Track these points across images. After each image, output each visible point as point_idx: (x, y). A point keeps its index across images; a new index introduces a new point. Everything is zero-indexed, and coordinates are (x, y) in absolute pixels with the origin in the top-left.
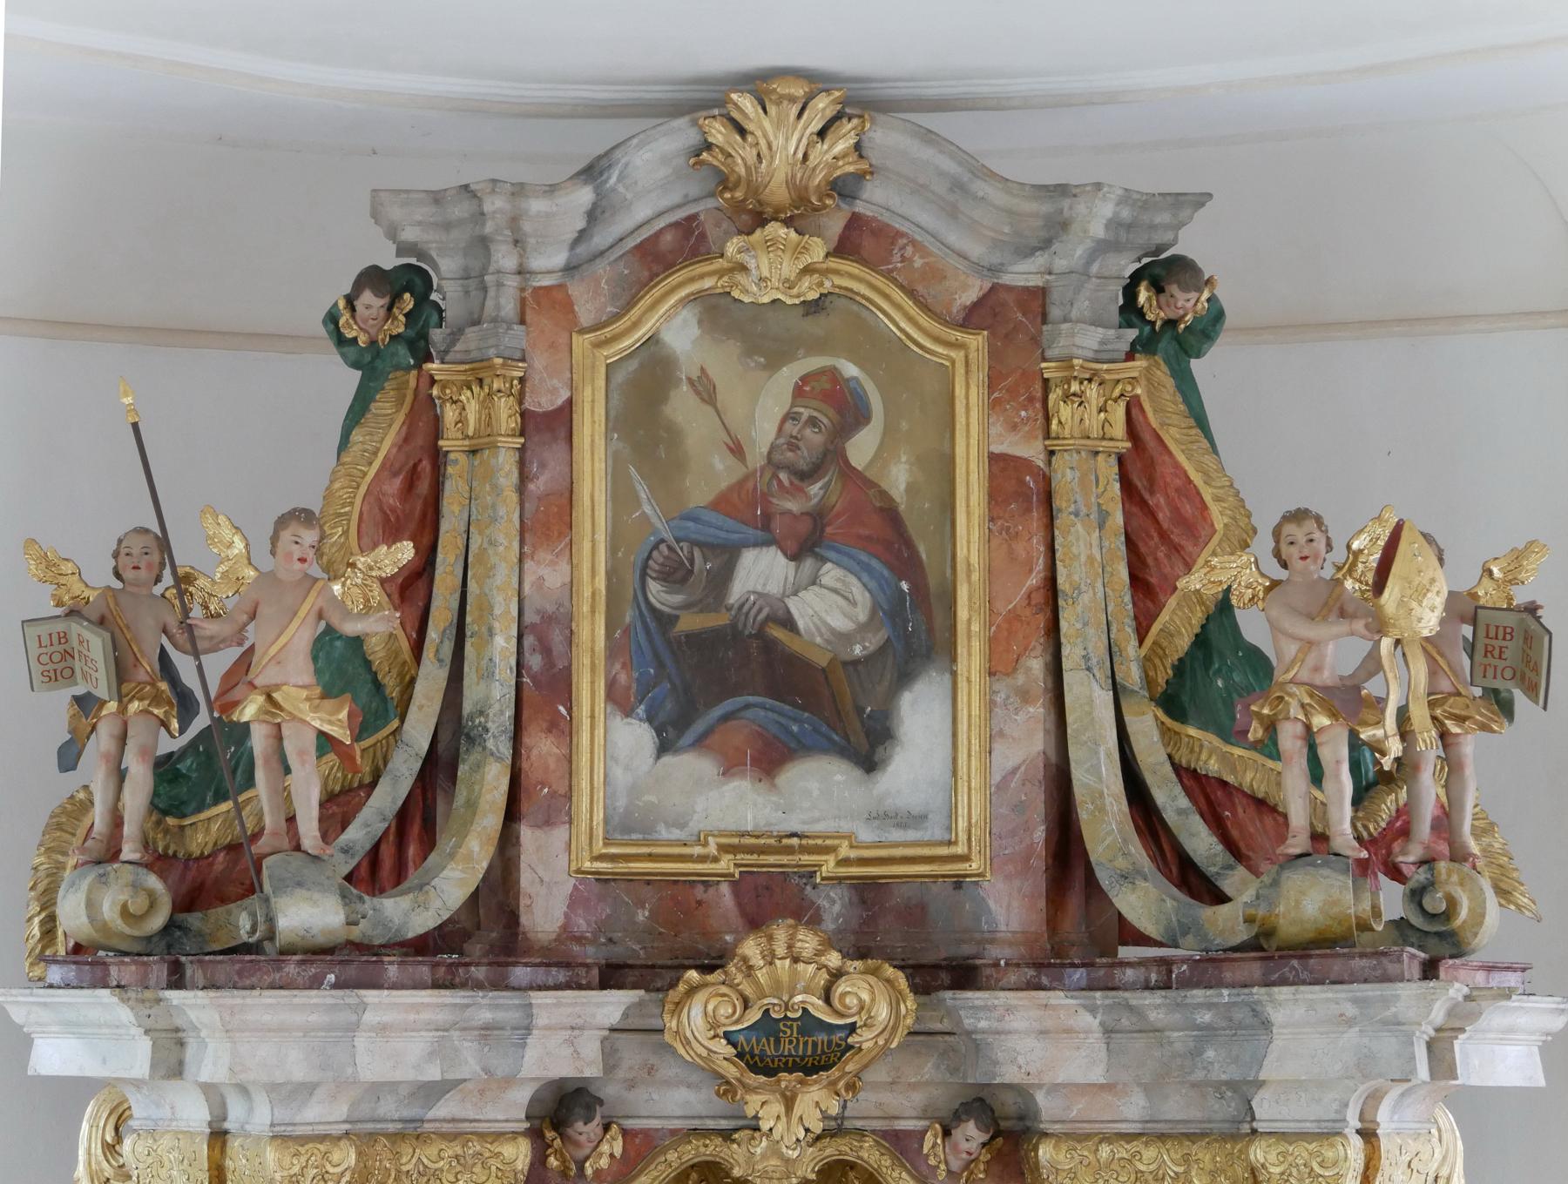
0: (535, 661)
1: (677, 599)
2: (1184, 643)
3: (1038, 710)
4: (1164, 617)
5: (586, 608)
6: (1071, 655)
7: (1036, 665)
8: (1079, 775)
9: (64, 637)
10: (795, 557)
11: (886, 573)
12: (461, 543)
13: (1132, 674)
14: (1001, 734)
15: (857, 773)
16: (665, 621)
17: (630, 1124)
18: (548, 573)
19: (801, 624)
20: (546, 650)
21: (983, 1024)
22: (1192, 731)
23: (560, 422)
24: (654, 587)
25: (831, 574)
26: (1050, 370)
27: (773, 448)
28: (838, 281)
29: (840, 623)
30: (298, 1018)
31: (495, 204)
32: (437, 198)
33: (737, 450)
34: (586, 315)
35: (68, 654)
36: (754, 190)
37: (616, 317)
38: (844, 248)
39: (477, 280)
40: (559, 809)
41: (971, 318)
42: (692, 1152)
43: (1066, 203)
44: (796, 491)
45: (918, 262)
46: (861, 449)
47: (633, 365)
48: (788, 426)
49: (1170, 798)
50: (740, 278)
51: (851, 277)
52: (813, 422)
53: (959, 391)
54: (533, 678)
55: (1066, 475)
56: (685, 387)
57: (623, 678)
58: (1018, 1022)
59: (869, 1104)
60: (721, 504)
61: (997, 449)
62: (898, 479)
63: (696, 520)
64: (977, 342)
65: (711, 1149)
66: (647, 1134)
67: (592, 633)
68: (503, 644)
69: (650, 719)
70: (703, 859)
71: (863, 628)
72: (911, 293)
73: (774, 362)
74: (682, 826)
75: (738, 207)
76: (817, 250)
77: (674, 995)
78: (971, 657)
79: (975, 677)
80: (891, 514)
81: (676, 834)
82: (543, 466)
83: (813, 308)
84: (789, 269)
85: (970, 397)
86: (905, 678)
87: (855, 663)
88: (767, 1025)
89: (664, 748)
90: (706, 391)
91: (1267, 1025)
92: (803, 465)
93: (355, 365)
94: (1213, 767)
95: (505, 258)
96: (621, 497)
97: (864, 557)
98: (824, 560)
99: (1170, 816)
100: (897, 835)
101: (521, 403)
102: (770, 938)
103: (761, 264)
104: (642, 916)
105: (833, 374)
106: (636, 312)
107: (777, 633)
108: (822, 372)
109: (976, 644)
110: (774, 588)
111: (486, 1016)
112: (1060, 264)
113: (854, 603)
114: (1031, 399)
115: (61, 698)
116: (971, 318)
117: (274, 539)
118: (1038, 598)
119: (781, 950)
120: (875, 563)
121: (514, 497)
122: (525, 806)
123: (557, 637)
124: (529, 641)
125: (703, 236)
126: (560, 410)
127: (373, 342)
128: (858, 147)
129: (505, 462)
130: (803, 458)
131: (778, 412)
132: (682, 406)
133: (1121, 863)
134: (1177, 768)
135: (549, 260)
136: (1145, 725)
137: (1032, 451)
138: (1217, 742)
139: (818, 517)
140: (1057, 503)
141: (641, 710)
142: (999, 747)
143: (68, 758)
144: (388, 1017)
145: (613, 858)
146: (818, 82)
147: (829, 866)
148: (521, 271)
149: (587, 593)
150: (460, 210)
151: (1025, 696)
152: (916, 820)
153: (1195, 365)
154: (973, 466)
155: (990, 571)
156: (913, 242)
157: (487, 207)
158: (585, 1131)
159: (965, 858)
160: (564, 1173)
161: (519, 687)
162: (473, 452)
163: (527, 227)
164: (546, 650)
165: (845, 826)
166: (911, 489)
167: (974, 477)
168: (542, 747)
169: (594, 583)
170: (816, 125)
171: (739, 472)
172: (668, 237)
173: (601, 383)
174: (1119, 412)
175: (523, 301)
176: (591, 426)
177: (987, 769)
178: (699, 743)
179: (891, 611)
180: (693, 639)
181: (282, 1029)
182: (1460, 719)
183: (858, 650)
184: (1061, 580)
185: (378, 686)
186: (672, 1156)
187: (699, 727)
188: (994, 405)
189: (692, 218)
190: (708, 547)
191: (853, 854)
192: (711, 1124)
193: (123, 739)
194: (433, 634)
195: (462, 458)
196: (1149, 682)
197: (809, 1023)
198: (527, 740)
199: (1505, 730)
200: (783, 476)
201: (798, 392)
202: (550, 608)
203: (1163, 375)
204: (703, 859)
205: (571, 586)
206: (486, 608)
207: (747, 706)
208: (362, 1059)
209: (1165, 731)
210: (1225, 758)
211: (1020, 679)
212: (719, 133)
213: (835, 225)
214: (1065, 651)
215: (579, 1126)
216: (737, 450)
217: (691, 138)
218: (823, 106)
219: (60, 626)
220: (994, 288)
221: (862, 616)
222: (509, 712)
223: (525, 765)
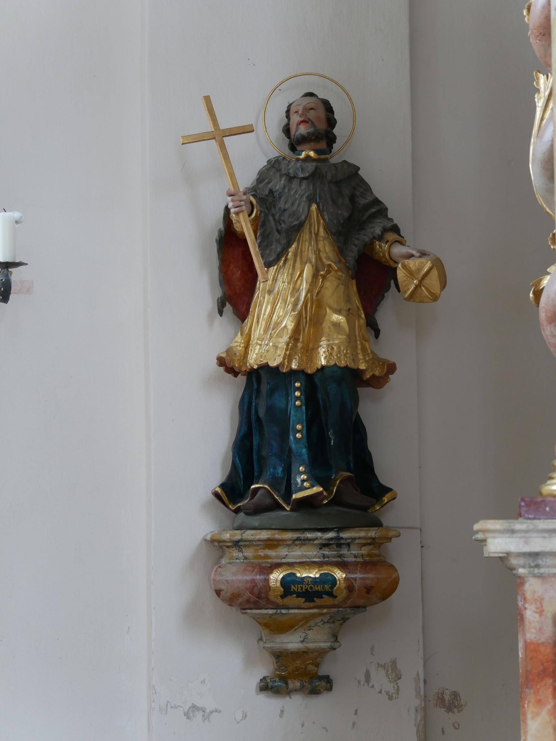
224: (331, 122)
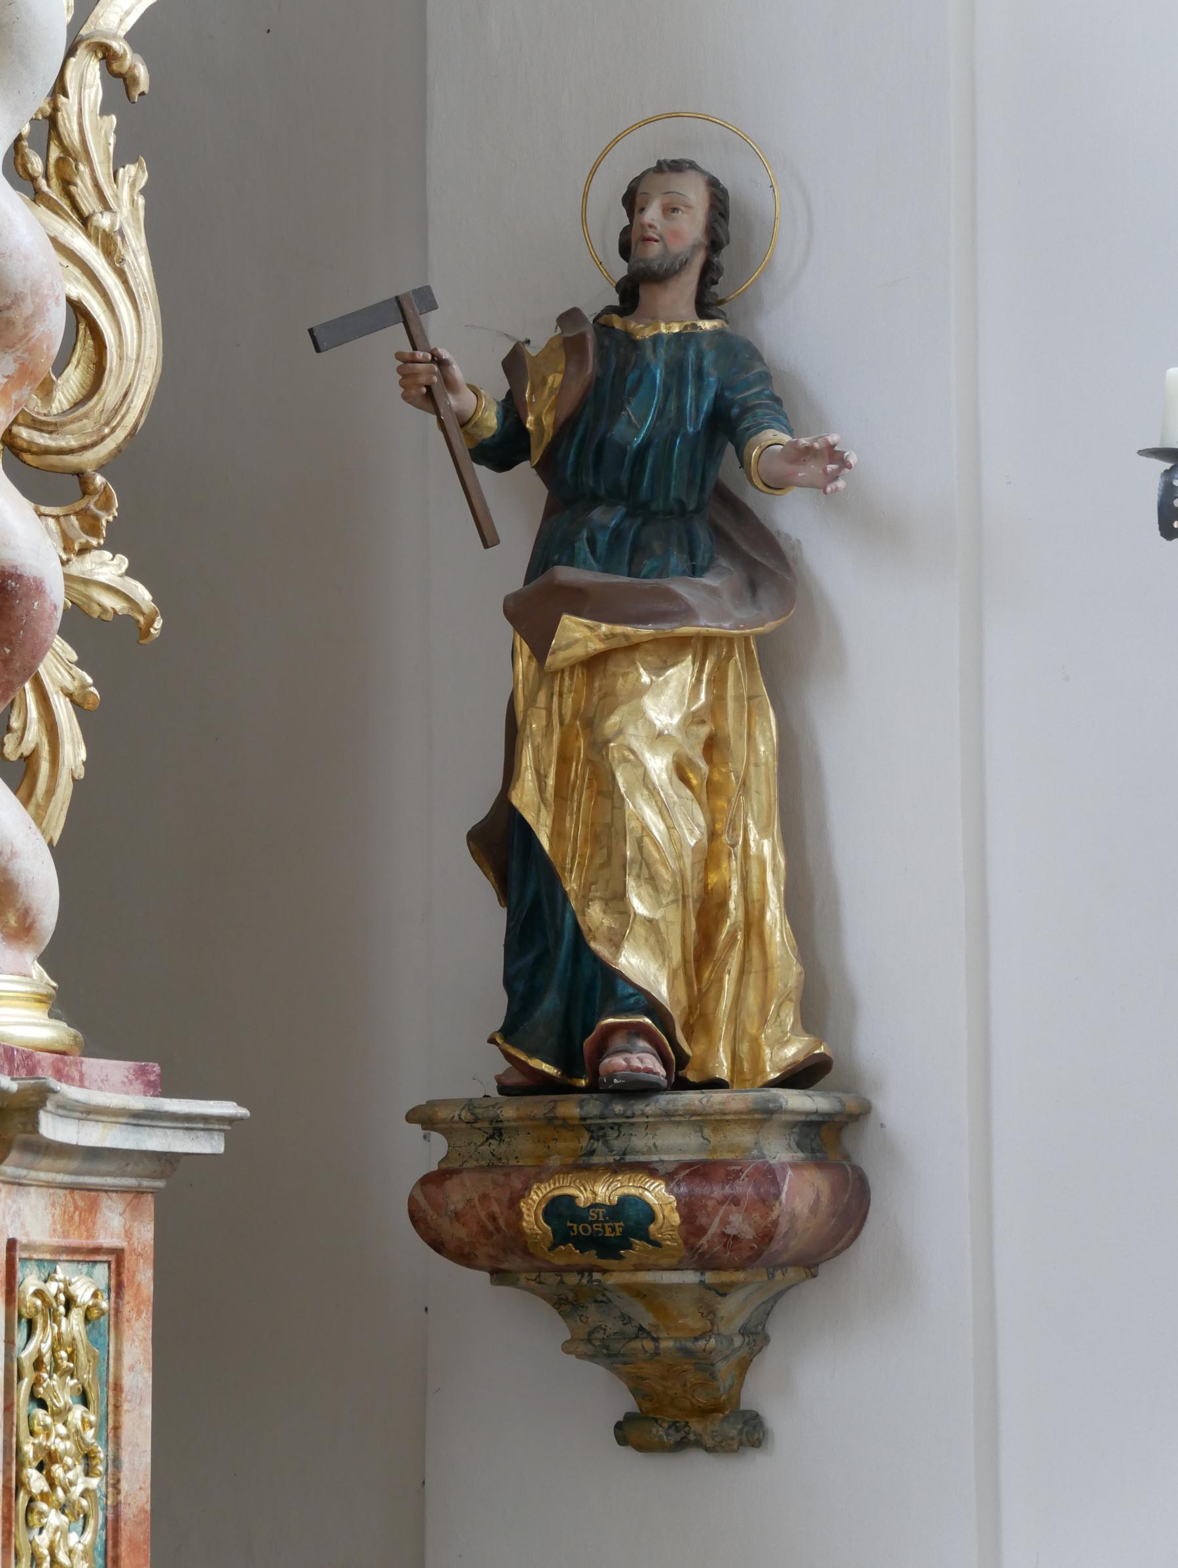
8: (129, 305)
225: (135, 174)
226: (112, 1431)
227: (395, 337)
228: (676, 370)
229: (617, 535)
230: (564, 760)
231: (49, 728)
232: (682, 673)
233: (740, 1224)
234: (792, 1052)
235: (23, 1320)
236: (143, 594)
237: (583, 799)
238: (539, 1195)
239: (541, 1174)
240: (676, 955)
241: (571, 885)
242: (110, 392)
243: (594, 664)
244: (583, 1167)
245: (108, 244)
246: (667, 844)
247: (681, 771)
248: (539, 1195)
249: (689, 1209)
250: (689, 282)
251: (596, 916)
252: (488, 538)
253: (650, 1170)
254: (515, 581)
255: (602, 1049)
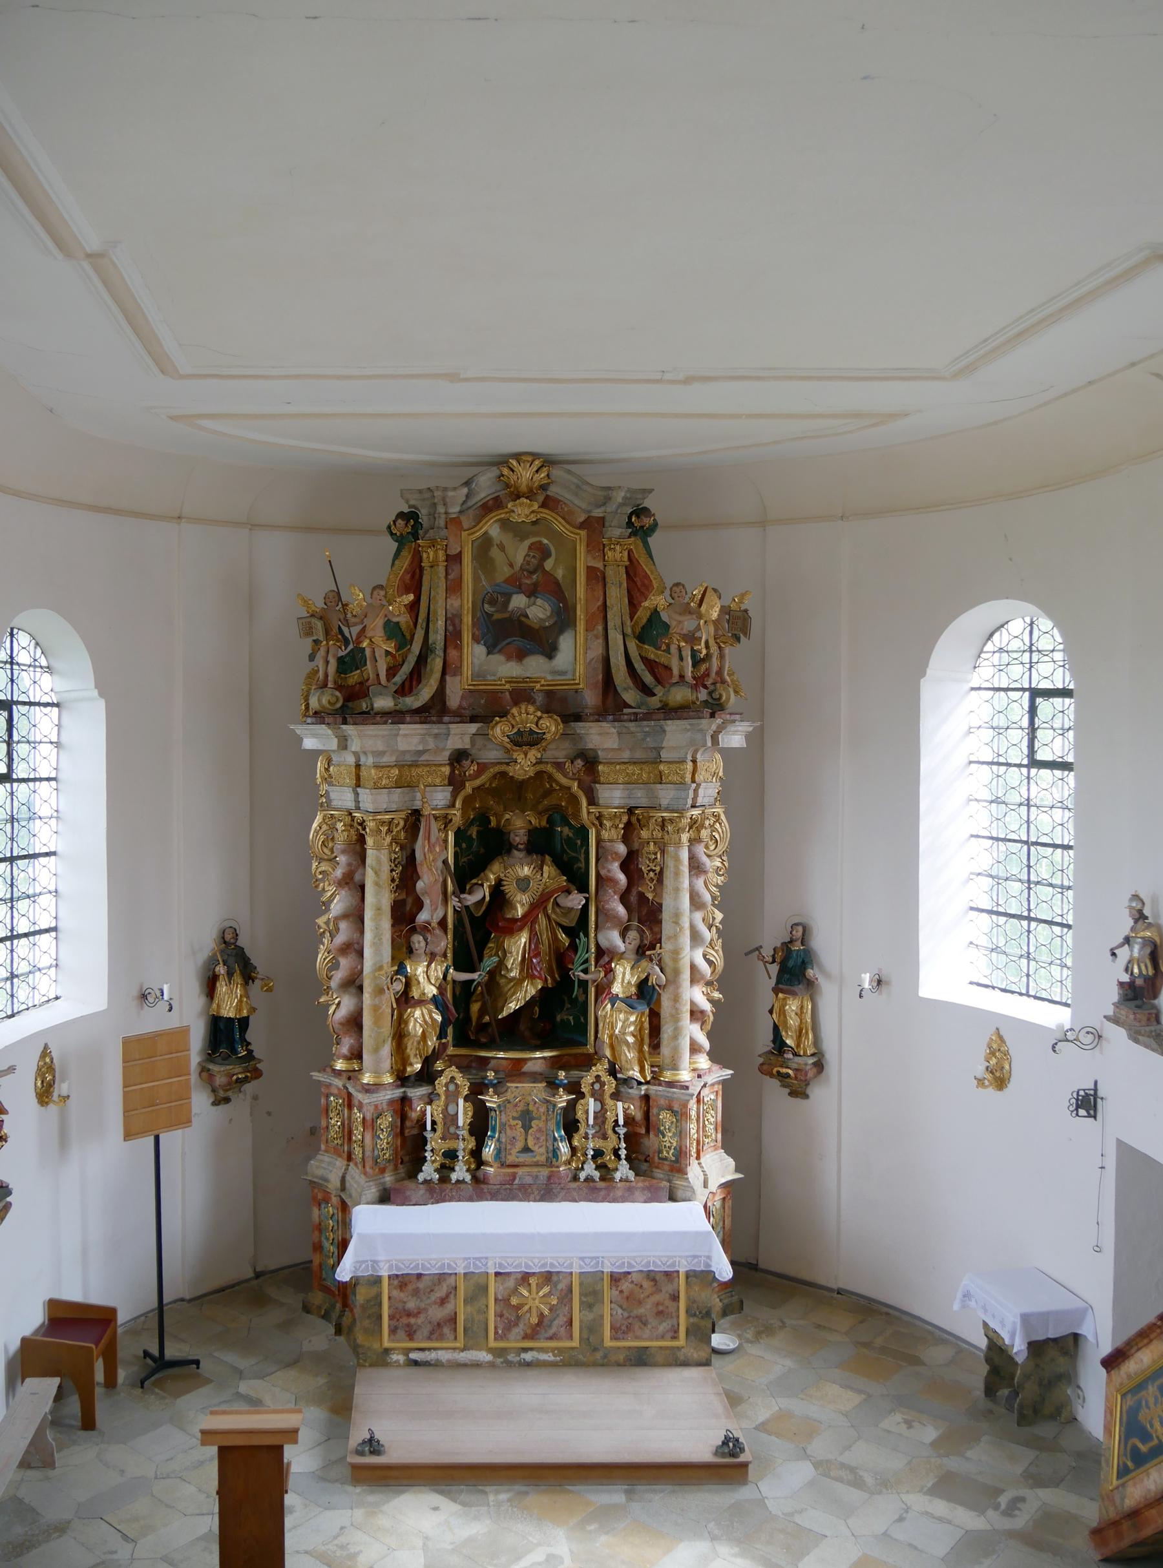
0: (450, 628)
1: (493, 609)
2: (644, 621)
3: (600, 641)
4: (638, 613)
5: (466, 612)
6: (610, 624)
7: (600, 628)
8: (612, 660)
9: (310, 623)
10: (528, 597)
11: (556, 601)
12: (428, 594)
13: (629, 630)
14: (590, 648)
15: (547, 660)
16: (489, 615)
17: (479, 761)
18: (454, 602)
19: (530, 617)
20: (454, 625)
21: (583, 732)
22: (646, 646)
23: (457, 558)
24: (486, 606)
25: (539, 602)
26: (605, 541)
27: (522, 564)
28: (544, 515)
29: (542, 616)
30: (381, 733)
31: (437, 494)
32: (420, 491)
33: (511, 565)
34: (465, 525)
35: (311, 628)
36: (516, 488)
37: (475, 526)
38: (544, 505)
39: (433, 515)
40: (458, 671)
41: (582, 526)
42: (497, 769)
43: (610, 492)
44: (528, 577)
45: (566, 509)
46: (549, 565)
47: (480, 540)
48: (527, 558)
49: (639, 666)
50: (512, 514)
51: (546, 514)
52: (534, 557)
53: (578, 548)
54: (450, 633)
55: (610, 572)
56: (495, 547)
57: (477, 633)
58: (592, 731)
59: (549, 755)
60: (507, 581)
61: (589, 565)
62: (560, 574)
63: (499, 586)
64: (583, 533)
65: (503, 768)
66: (484, 763)
67: (467, 620)
68: (441, 623)
69: (485, 645)
70: (501, 685)
71: (549, 617)
72: (564, 518)
73: (522, 539)
74: (494, 676)
75: (512, 493)
76: (536, 506)
77: (491, 725)
78: (581, 626)
79: (582, 631)
80: (557, 583)
81: (493, 678)
82: (453, 570)
83: (534, 523)
84: (527, 511)
85: (581, 550)
86: (561, 631)
87: (547, 627)
88: (519, 733)
89: (489, 653)
90: (502, 547)
91: (664, 731)
92: (531, 570)
93: (396, 541)
94: (652, 657)
95: (441, 509)
96: (476, 579)
97: (549, 596)
98: (537, 598)
99: (639, 671)
100: (558, 677)
101: (446, 552)
102: (520, 708)
103: (519, 510)
104: (483, 702)
105: (540, 542)
106: (481, 524)
107: (523, 619)
108: (537, 542)
109: (582, 622)
110: (522, 606)
111: (436, 731)
112: (609, 510)
113: (546, 610)
114: (599, 550)
115: (309, 641)
116: (582, 526)
117: (372, 594)
118: (601, 608)
119: (523, 711)
120: (553, 599)
121: (444, 580)
122: (447, 671)
123: (457, 621)
124: (448, 622)
125: (501, 502)
126: (458, 554)
127: (401, 534)
128: (548, 475)
129: (441, 569)
130: (531, 568)
131: (524, 554)
132: (495, 553)
133: (625, 685)
134: (642, 657)
135: (454, 510)
136: (632, 645)
137: (600, 565)
138: (654, 650)
139: (535, 585)
140: (607, 580)
141: (482, 642)
142: (588, 651)
143: (312, 658)
144: (407, 732)
145: (474, 685)
146: (535, 456)
147: (538, 686)
148: (446, 513)
149: (466, 608)
150: (427, 495)
151: (597, 637)
152: (564, 673)
153: (649, 539)
154: (582, 570)
155: (587, 600)
156: (565, 503)
157: (435, 495)
158: (466, 763)
159: (579, 684)
160: (460, 775)
161: (446, 636)
162: (432, 567)
163: (448, 500)
164: (454, 625)
165: (543, 675)
166: (563, 576)
167: (582, 573)
168: (453, 653)
169: (468, 604)
170: (535, 469)
171: (512, 571)
172: (491, 502)
173: (470, 546)
174: (626, 553)
175: (447, 522)
176: (467, 559)
177: (585, 658)
178: (500, 652)
179: (557, 612)
180: (499, 621)
181: (375, 736)
182: (724, 643)
183: (547, 624)
184: (608, 603)
185: (403, 635)
186: (492, 770)
187: (499, 647)
188: (588, 552)
189: (498, 496)
190: (503, 594)
191: (545, 683)
192: (503, 761)
193: (328, 652)
194: (420, 620)
195: (428, 569)
196: (634, 632)
197: (531, 732)
198: (448, 651)
199: (738, 645)
200: (525, 573)
201: (530, 548)
202: (455, 613)
203: (639, 542)
204: (501, 685)
205: (461, 606)
206: (436, 613)
207: (514, 641)
208: (400, 744)
209: (638, 646)
210: (656, 654)
211: (595, 632)
212: (506, 471)
213: (541, 498)
214: (609, 624)
215: (464, 762)
216: (511, 565)
217: (497, 472)
218: (537, 463)
219: (309, 620)
220: (589, 517)
221: (548, 614)
222: (443, 644)
223: (448, 658)
224: (237, 935)
225: (720, 940)
226: (716, 1113)
227: (757, 952)
228: (797, 955)
229: (788, 979)
230: (780, 1011)
231: (458, 719)
232: (796, 1002)
233: (802, 1078)
234: (812, 1052)
235: (359, 1160)
236: (721, 996)
237: (782, 1017)
238: (775, 1069)
239: (776, 1067)
240: (795, 1038)
241: (780, 1028)
242: (717, 971)
243: (784, 999)
244: (782, 1066)
245: (716, 951)
246: (719, 1212)
247: (796, 1014)
248: (775, 1069)
249: (795, 1075)
250: (800, 940)
251: (783, 1033)
252: (770, 978)
253: (790, 1069)
254: (773, 985)
255: (784, 1052)
